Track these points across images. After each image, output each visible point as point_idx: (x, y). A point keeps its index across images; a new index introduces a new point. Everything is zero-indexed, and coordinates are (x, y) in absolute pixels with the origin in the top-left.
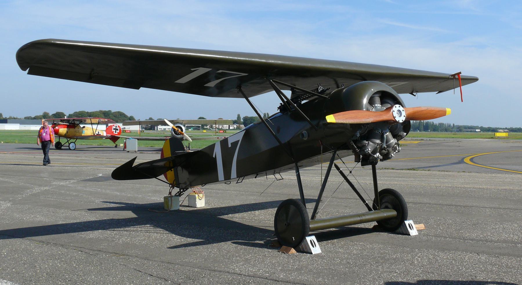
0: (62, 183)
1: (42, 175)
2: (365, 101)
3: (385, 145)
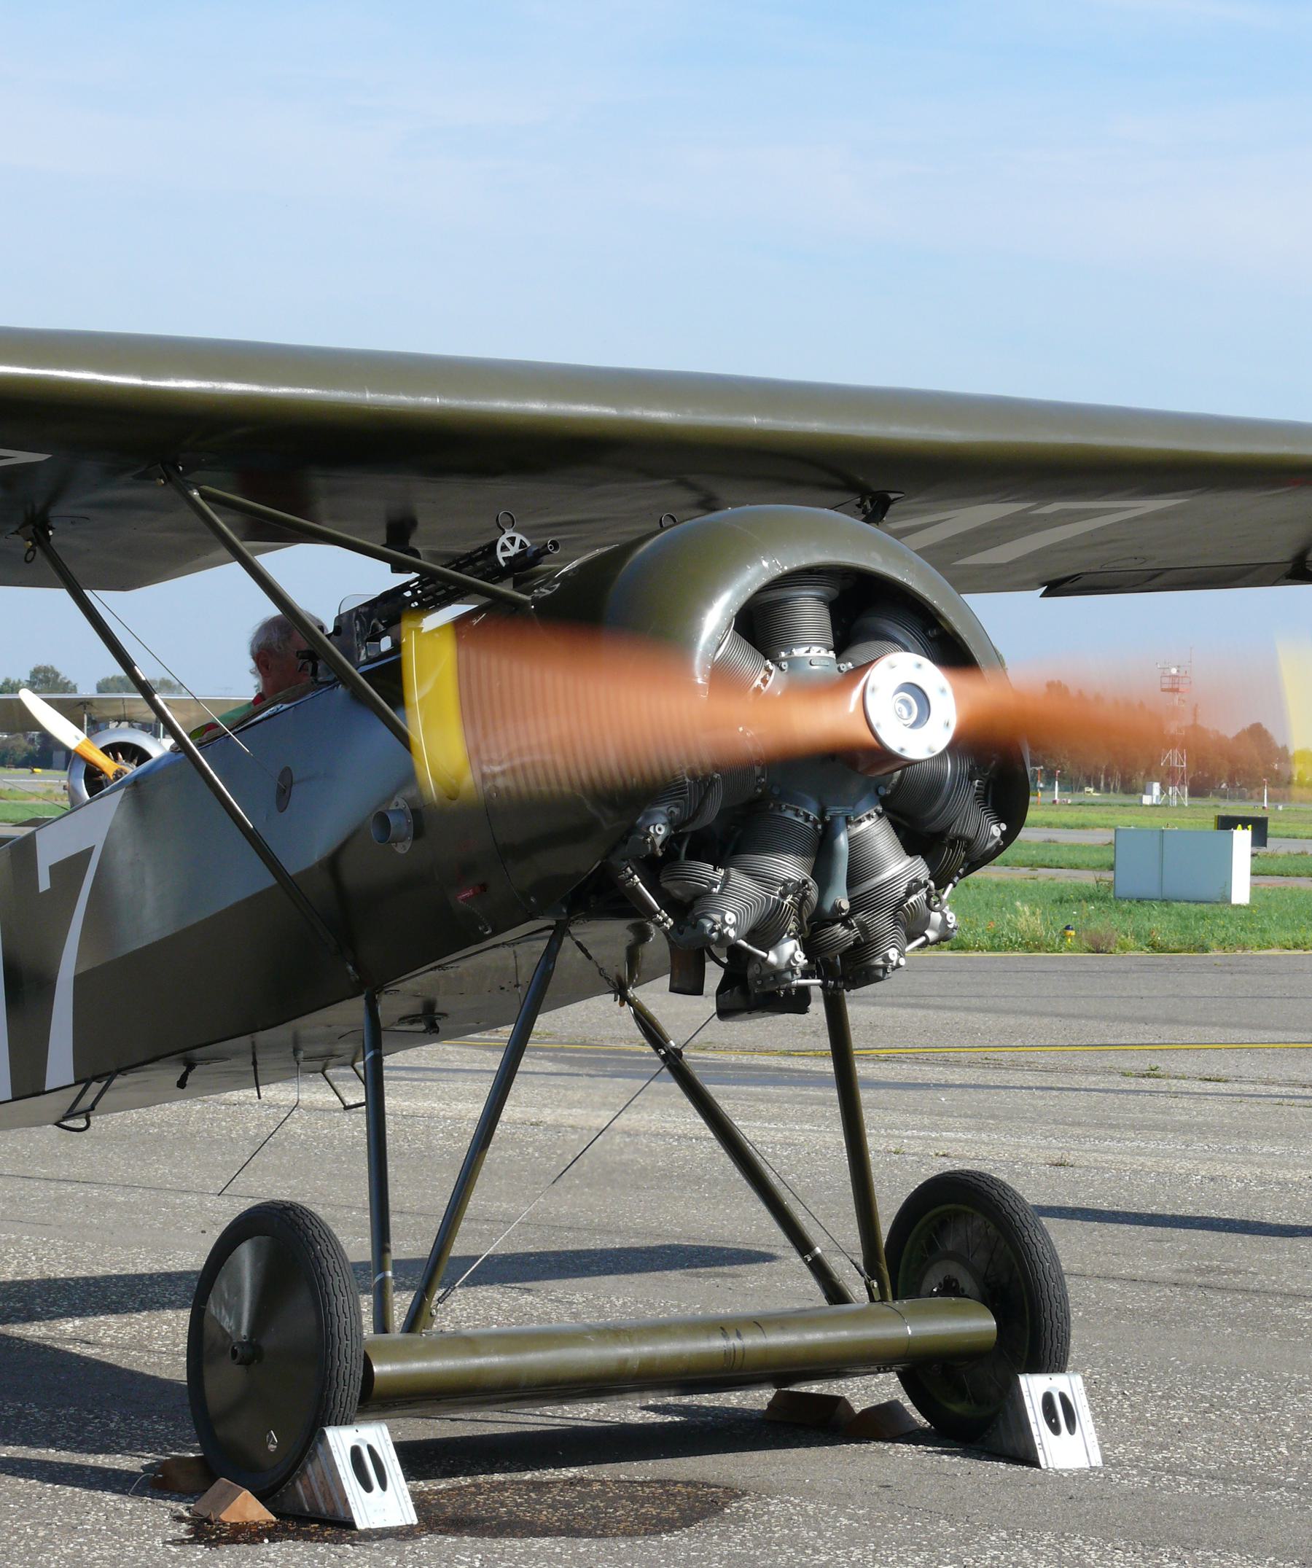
2: (716, 616)
3: (840, 897)
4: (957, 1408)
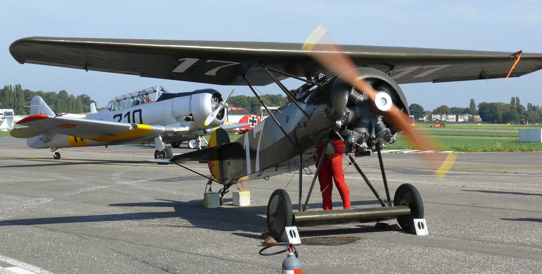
0: (127, 183)
4: (406, 225)
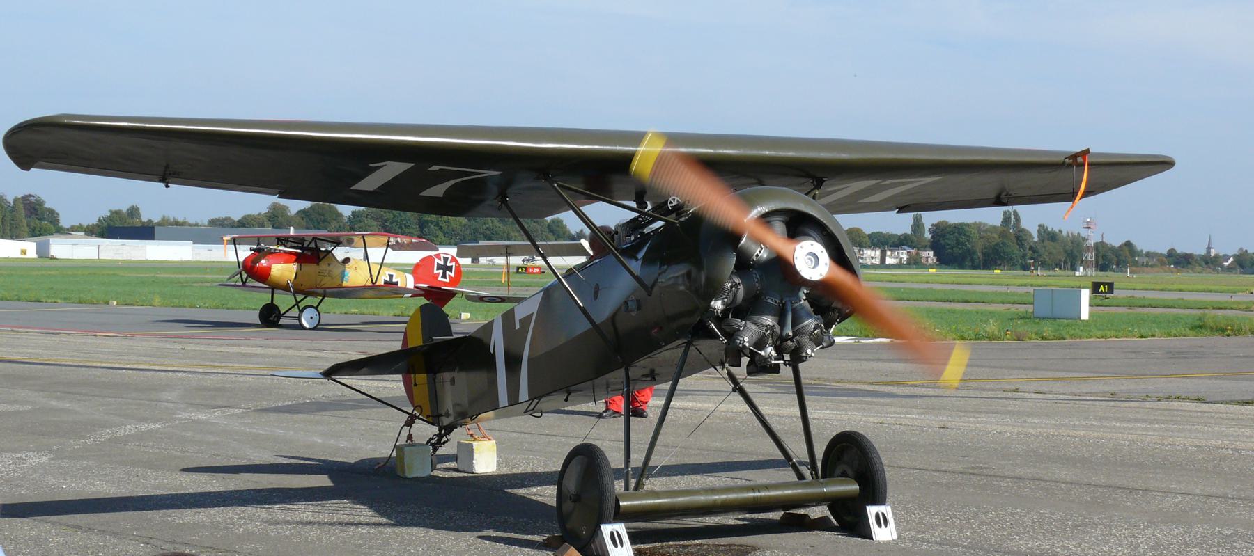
0: (202, 416)
1: (166, 395)
4: (848, 519)
